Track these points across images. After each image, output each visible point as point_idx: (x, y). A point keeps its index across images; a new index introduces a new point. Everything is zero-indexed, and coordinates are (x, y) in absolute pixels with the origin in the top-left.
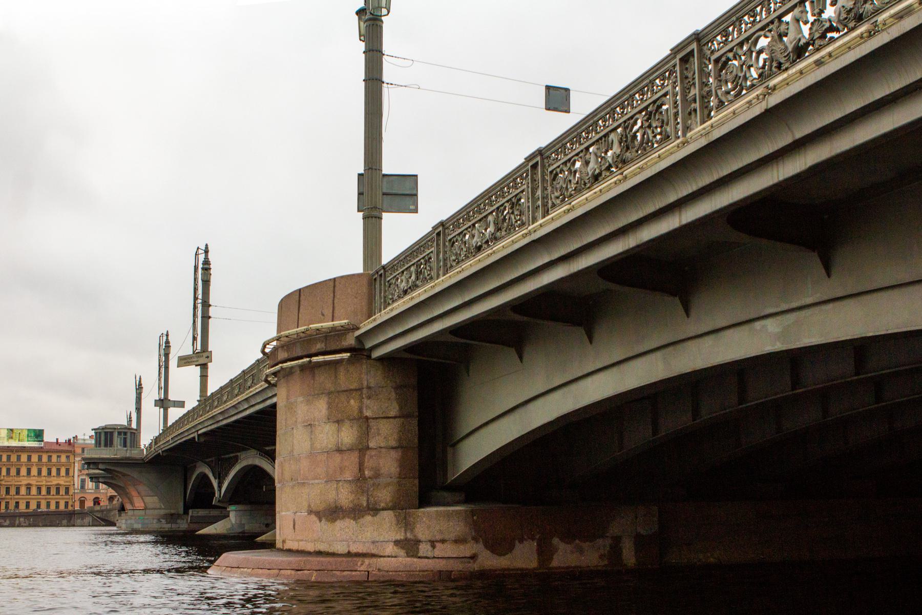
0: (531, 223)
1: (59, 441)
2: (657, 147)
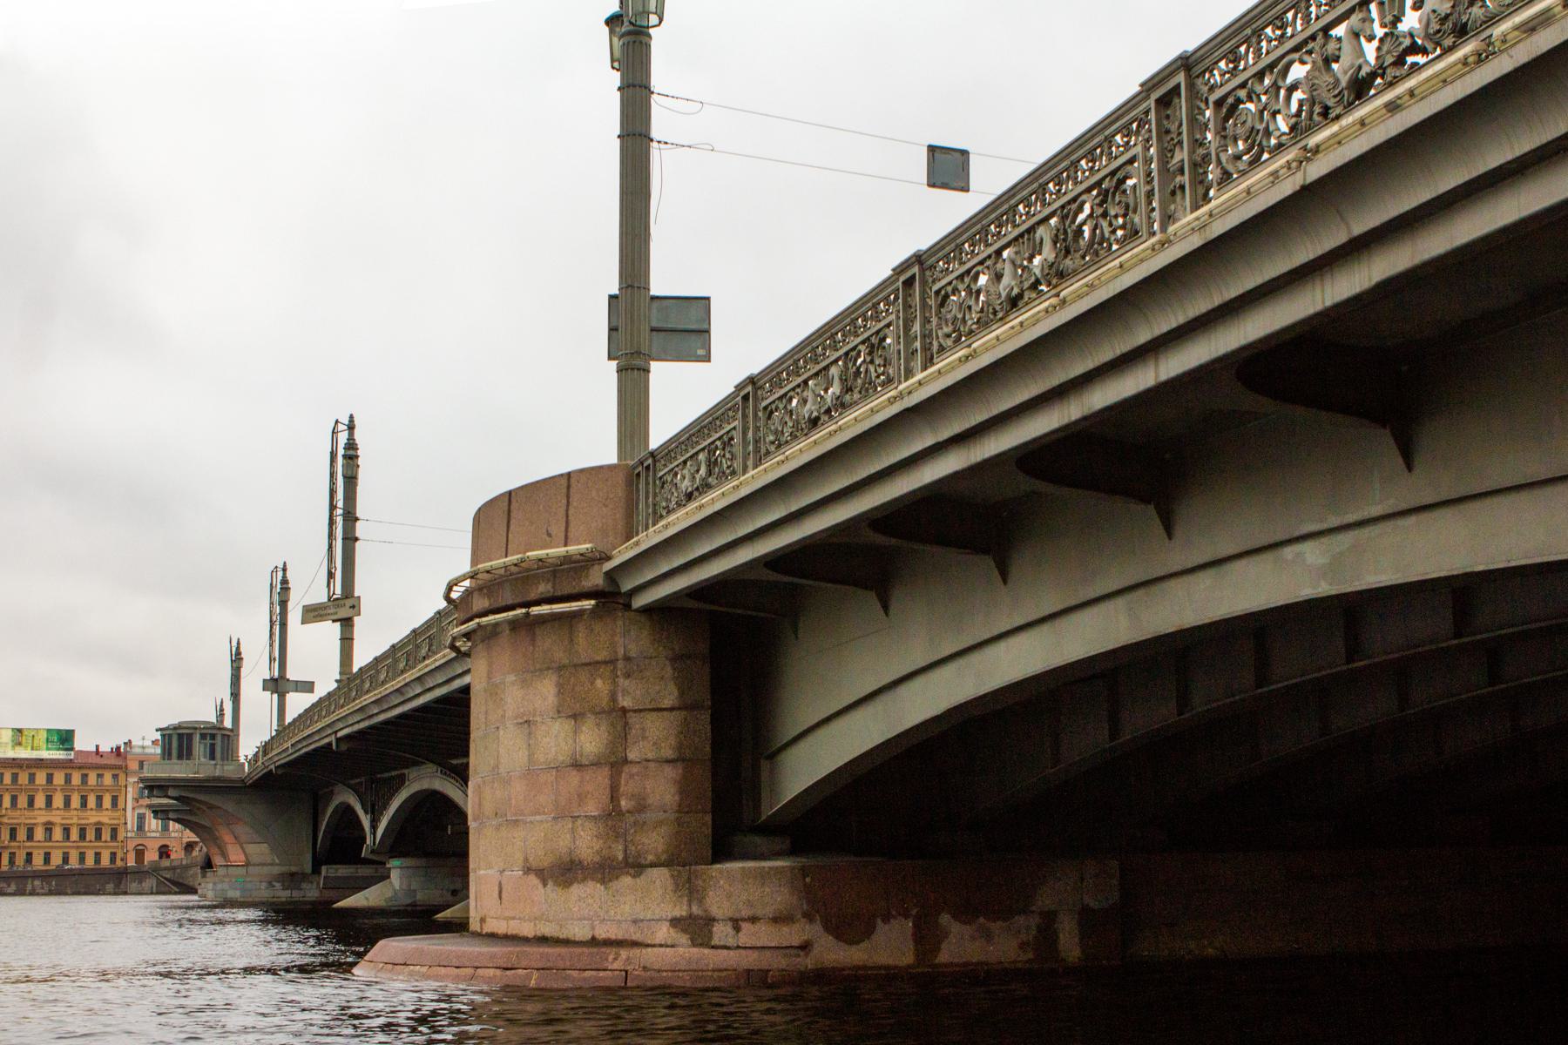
0: (903, 379)
1: (100, 750)
2: (1118, 250)
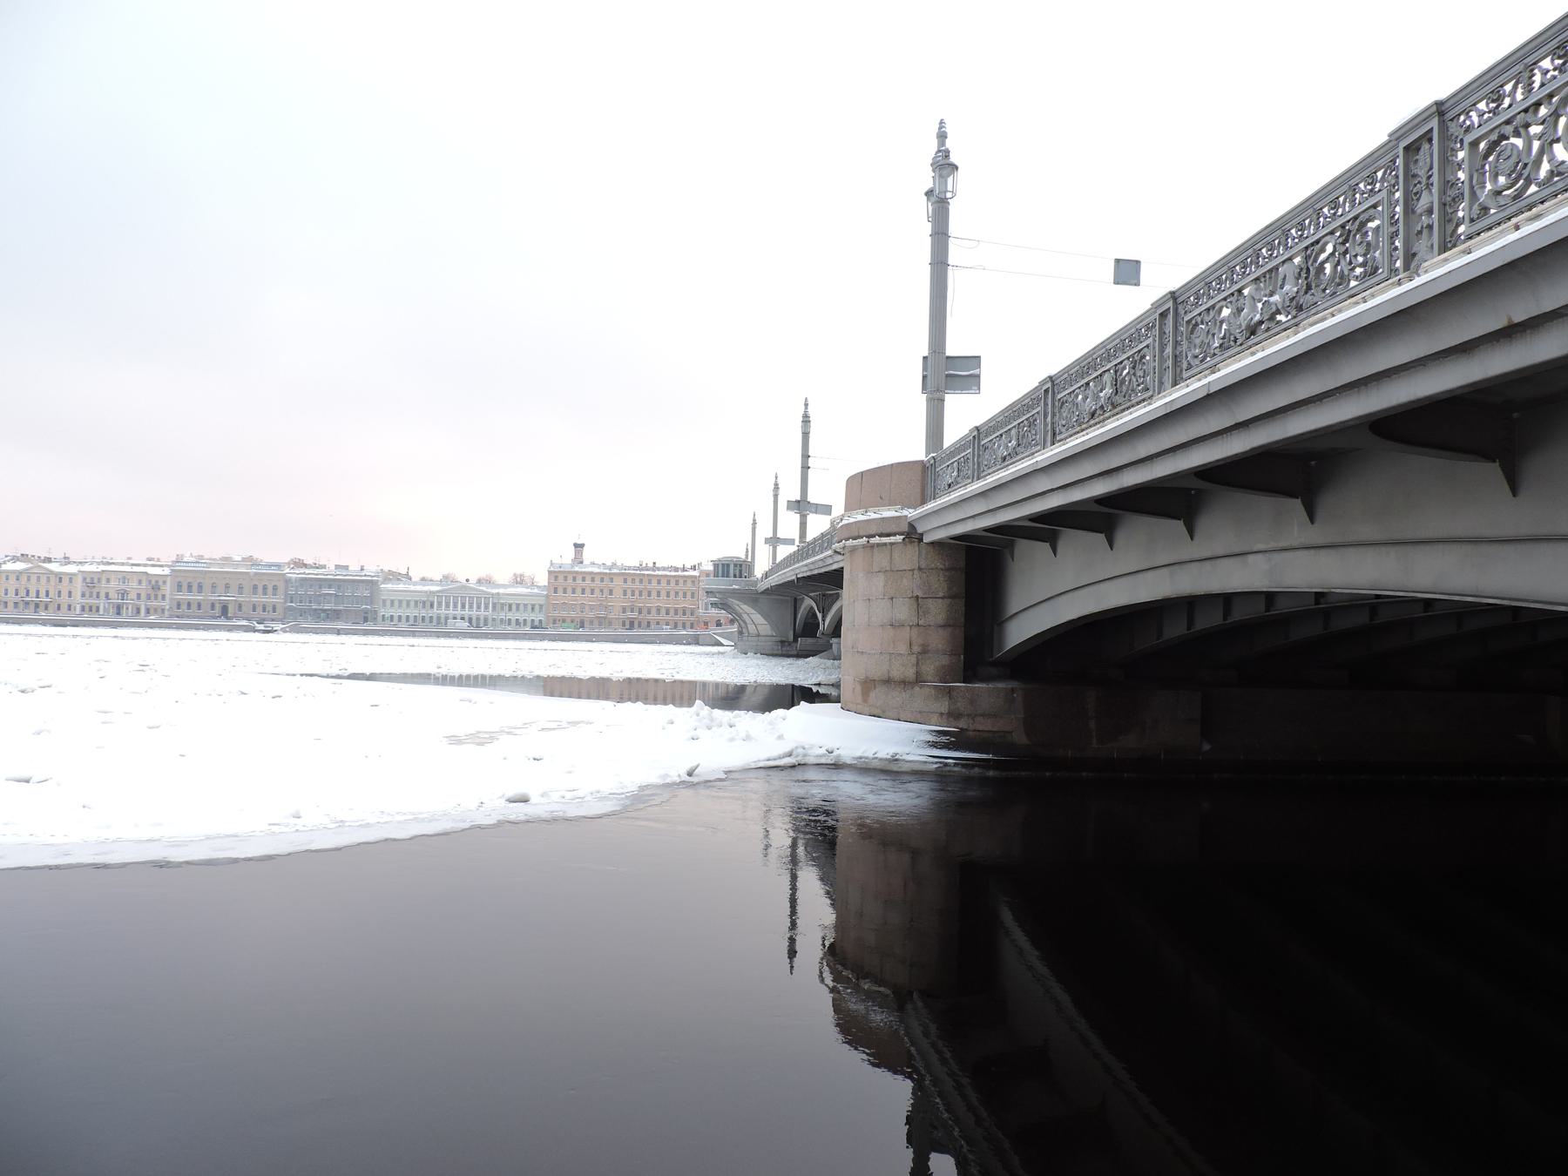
0: (1049, 444)
2: (1494, 214)
